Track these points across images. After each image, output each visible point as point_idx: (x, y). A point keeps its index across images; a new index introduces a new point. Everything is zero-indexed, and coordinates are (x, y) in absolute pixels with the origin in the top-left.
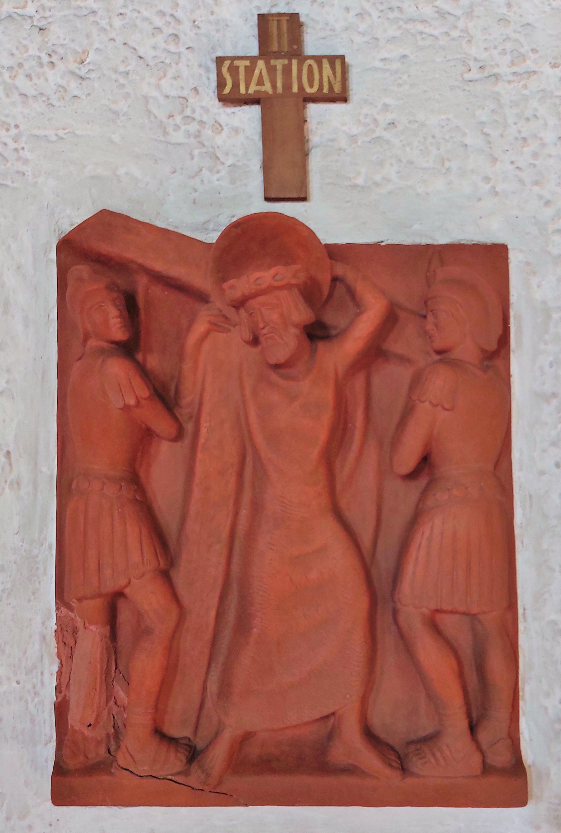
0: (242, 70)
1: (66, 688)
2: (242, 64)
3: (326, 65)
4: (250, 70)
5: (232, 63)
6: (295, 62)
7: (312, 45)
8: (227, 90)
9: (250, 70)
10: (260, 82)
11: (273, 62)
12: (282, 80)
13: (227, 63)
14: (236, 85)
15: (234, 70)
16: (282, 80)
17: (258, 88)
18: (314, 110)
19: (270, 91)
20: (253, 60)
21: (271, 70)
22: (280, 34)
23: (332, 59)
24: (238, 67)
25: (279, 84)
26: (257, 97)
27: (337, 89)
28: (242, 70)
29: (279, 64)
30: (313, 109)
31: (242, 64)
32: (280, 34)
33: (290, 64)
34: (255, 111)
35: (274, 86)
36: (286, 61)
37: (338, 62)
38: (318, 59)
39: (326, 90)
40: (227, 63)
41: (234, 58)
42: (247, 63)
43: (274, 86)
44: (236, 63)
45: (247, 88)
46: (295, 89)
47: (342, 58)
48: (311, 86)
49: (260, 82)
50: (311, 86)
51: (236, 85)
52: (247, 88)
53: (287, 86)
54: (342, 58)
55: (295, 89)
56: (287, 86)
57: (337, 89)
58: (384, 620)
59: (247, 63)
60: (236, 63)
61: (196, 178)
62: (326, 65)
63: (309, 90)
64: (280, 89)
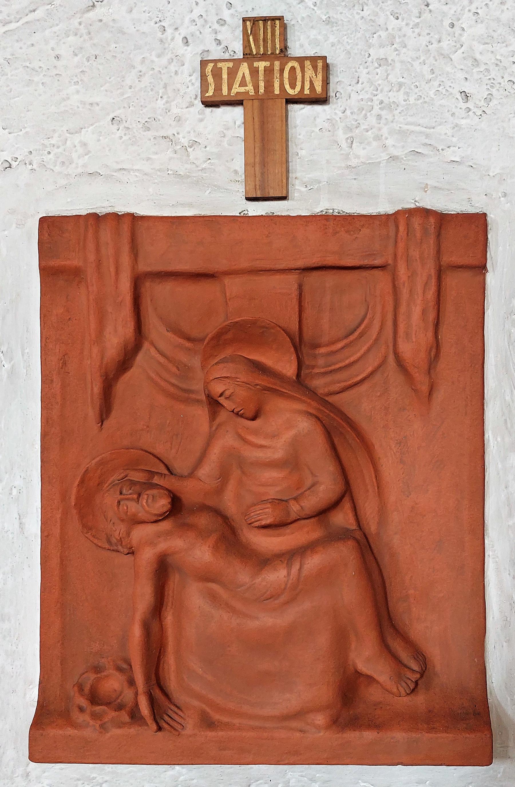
0: (225, 76)
1: (113, 56)
2: (225, 67)
3: (307, 63)
4: (232, 73)
5: (215, 66)
6: (277, 64)
7: (300, 45)
8: (210, 93)
9: (232, 73)
10: (243, 83)
11: (256, 64)
12: (268, 81)
13: (210, 66)
14: (218, 88)
15: (217, 74)
16: (268, 81)
17: (242, 89)
18: (299, 113)
19: (252, 93)
20: (237, 62)
21: (254, 72)
22: (265, 34)
23: (314, 60)
24: (221, 68)
25: (262, 84)
26: (240, 98)
27: (319, 89)
28: (225, 76)
29: (262, 65)
30: (294, 108)
31: (225, 67)
32: (265, 34)
33: (272, 65)
34: (238, 112)
35: (256, 88)
36: (268, 64)
37: (322, 65)
38: (301, 60)
39: (307, 92)
40: (210, 66)
41: (215, 61)
42: (231, 65)
43: (256, 88)
44: (220, 65)
45: (230, 89)
46: (277, 92)
47: (324, 58)
48: (293, 86)
49: (243, 83)
50: (293, 86)
51: (218, 88)
52: (230, 89)
53: (269, 85)
54: (324, 58)
55: (277, 92)
56: (269, 85)
57: (319, 89)
58: (363, 541)
59: (231, 65)
60: (220, 65)
61: (182, 168)
62: (307, 63)
63: (291, 92)
64: (262, 90)
